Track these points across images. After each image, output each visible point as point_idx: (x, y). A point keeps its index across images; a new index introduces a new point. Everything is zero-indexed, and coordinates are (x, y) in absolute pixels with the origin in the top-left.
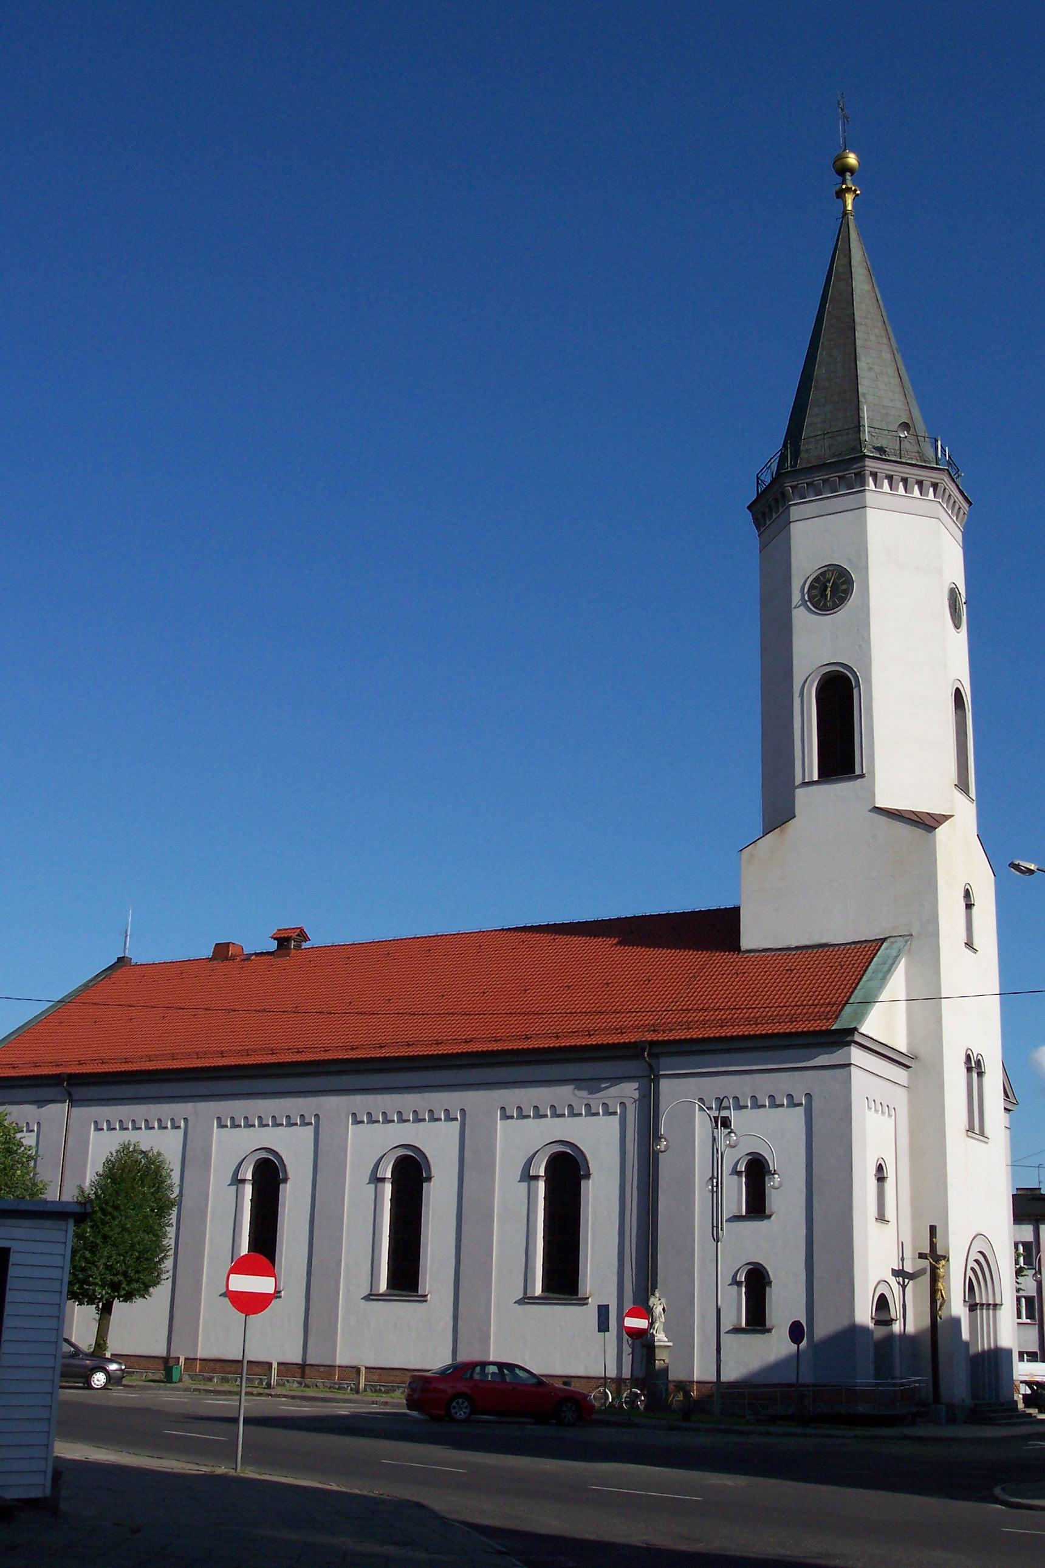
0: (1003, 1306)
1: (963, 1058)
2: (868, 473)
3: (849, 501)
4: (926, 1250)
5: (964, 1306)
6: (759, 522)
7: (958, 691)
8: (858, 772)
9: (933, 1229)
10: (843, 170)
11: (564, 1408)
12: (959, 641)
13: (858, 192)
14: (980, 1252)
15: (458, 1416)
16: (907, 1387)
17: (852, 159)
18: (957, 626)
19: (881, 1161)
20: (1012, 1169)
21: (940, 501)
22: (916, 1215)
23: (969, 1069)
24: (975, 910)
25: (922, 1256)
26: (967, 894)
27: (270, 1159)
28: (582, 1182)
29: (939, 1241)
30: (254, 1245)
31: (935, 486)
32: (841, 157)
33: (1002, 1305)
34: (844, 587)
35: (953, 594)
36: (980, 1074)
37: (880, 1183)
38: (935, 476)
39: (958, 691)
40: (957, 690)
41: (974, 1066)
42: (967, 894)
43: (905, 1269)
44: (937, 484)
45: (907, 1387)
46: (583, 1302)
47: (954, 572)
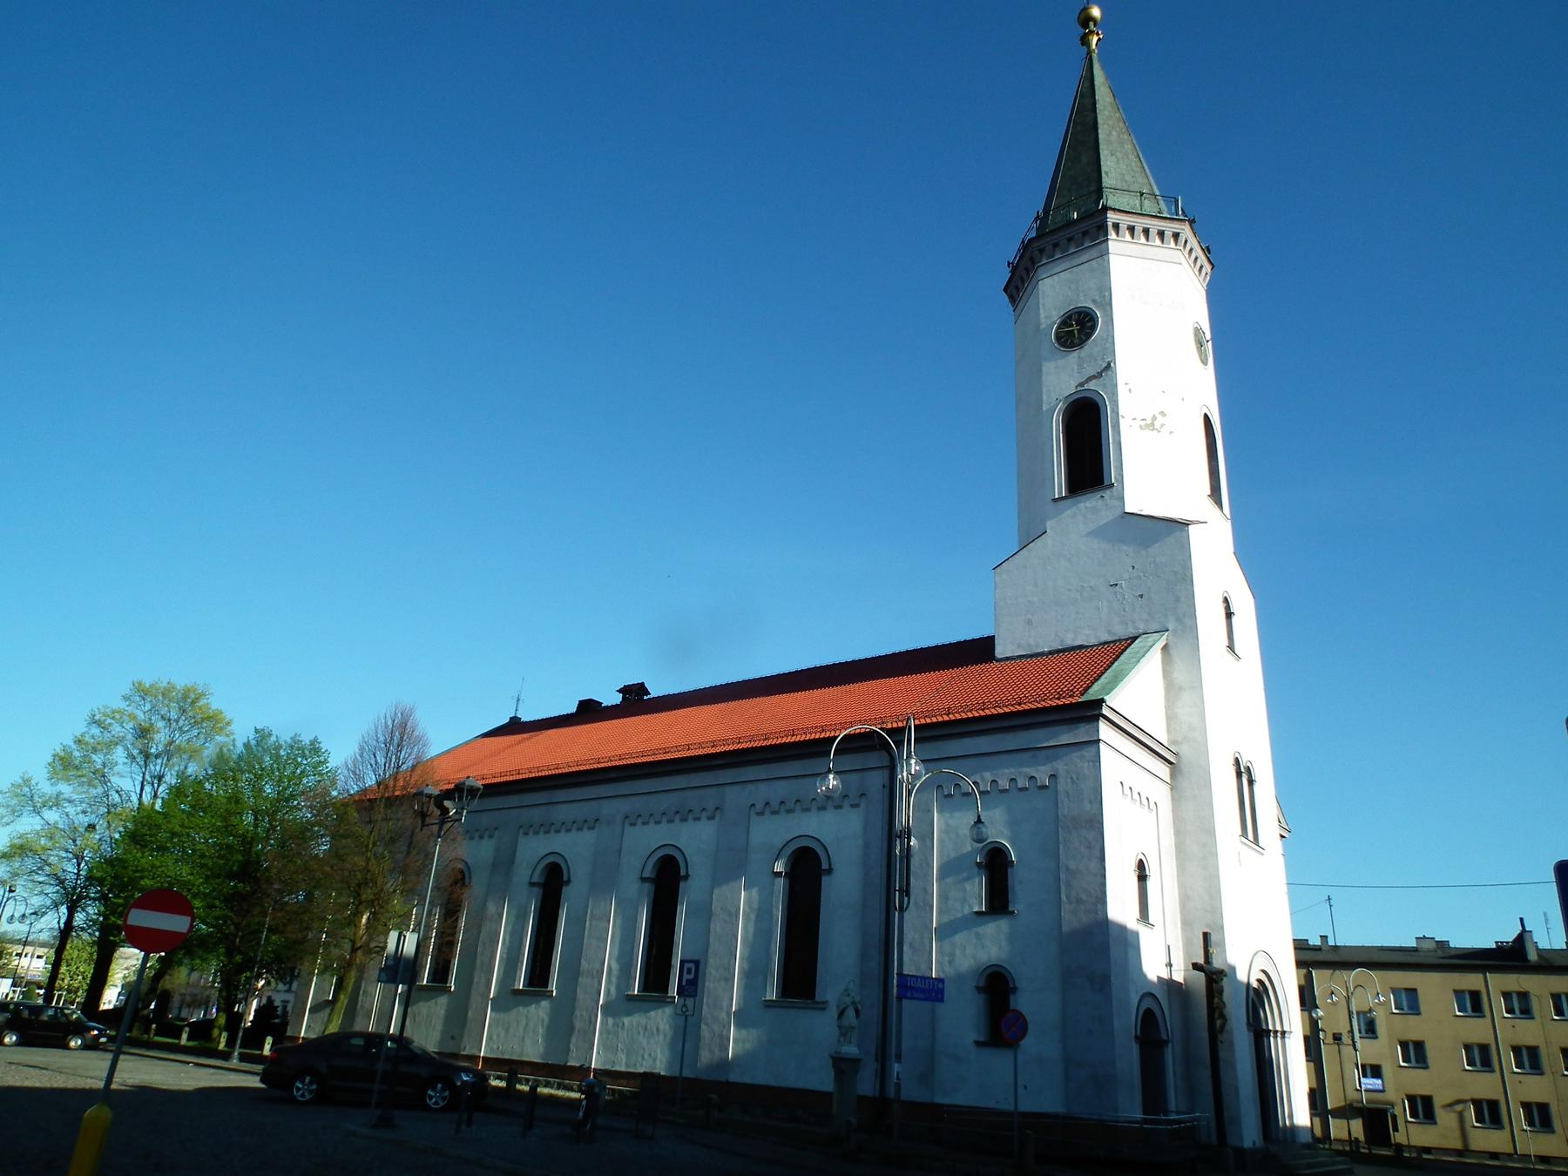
0: (1292, 1035)
1: (1232, 761)
2: (1110, 224)
3: (1094, 252)
4: (1201, 961)
5: (1249, 1030)
6: (1013, 299)
7: (1206, 416)
8: (1106, 483)
9: (1206, 936)
10: (1089, 19)
11: (308, 1079)
12: (1208, 374)
13: (1101, 37)
14: (1264, 971)
15: (431, 1103)
16: (1183, 1125)
17: (1096, 12)
18: (1205, 362)
19: (1226, 595)
20: (1288, 889)
21: (1182, 248)
22: (1186, 923)
23: (1239, 774)
24: (1234, 619)
25: (1196, 966)
26: (1141, 866)
27: (560, 867)
28: (824, 878)
29: (1213, 950)
30: (645, 986)
31: (1176, 236)
32: (1085, 9)
33: (1291, 1032)
34: (1089, 324)
35: (1198, 332)
36: (1251, 782)
37: (1141, 883)
38: (1176, 226)
39: (1206, 416)
40: (1206, 415)
41: (1243, 773)
42: (1141, 866)
43: (1174, 978)
44: (1179, 233)
45: (1183, 1125)
46: (822, 1007)
47: (1198, 312)
